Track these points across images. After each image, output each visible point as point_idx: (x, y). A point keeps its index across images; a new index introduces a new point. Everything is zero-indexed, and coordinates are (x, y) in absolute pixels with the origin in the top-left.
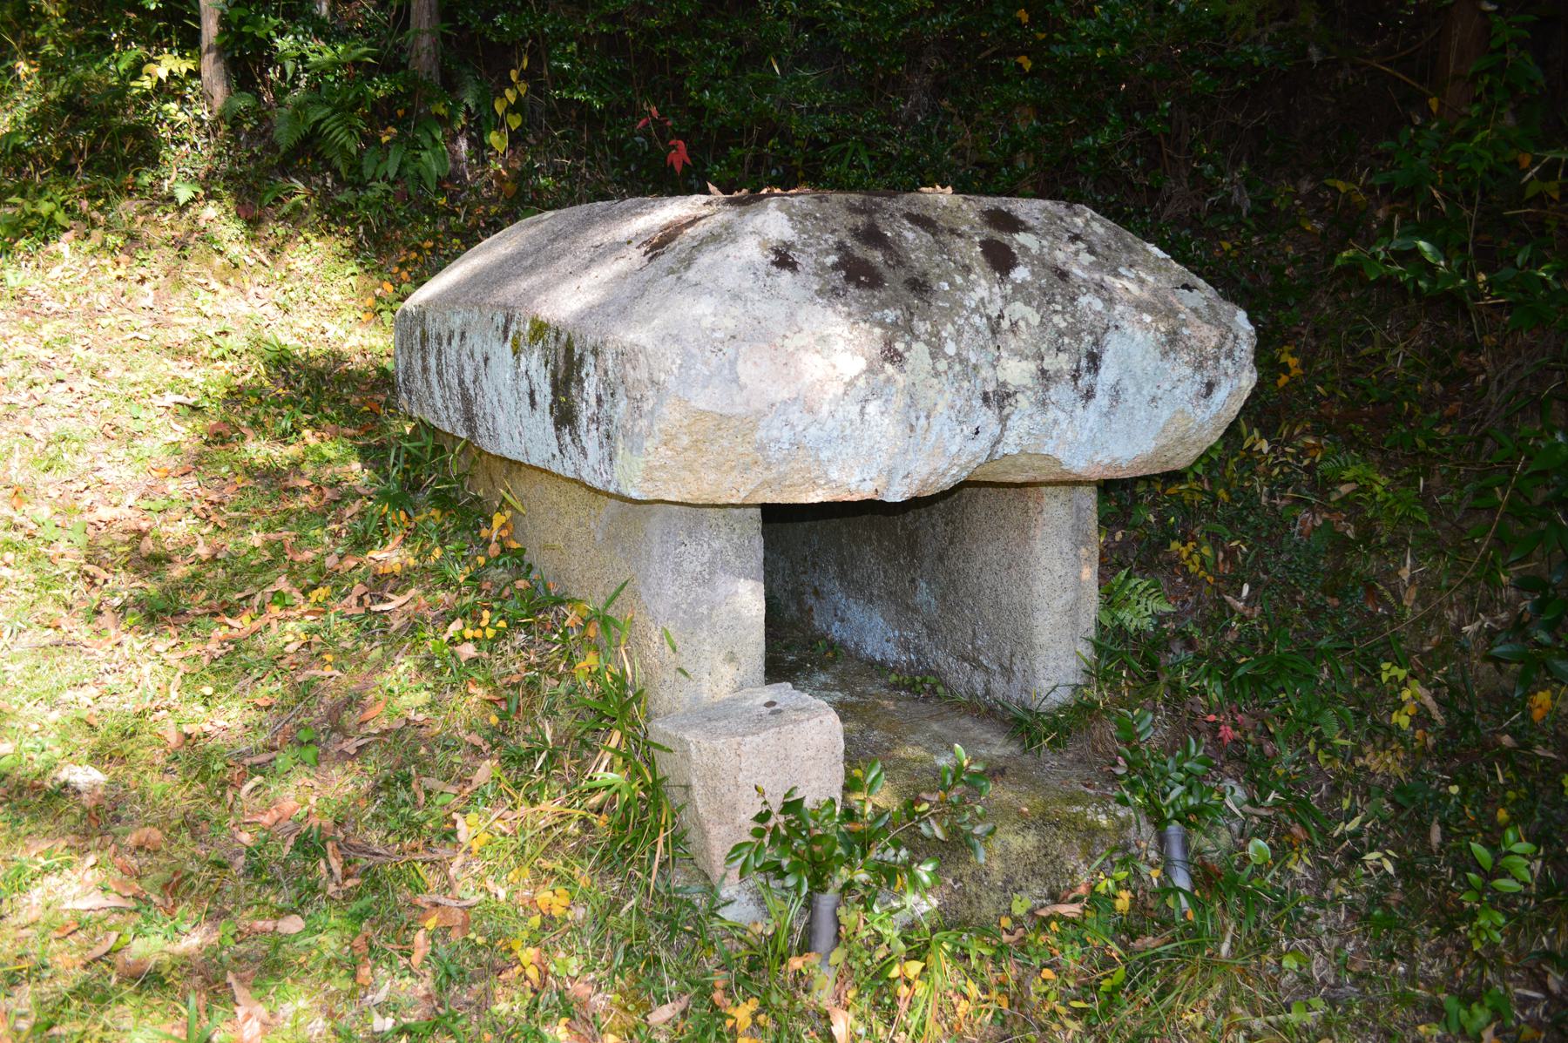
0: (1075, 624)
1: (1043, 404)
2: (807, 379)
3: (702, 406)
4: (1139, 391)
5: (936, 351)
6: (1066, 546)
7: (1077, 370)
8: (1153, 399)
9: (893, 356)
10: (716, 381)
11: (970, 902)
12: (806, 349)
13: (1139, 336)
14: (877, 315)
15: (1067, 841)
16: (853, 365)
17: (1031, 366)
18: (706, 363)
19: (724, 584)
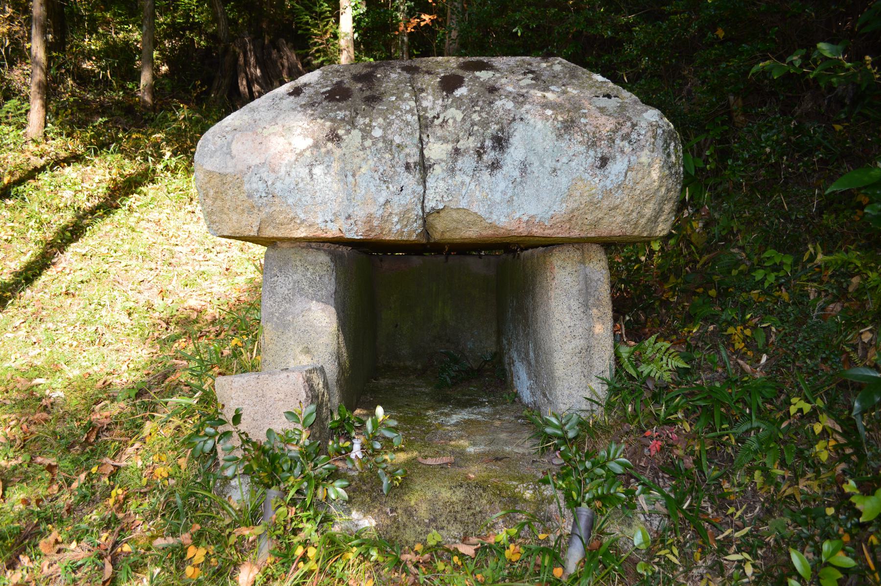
1: (452, 171)
2: (272, 151)
3: (209, 168)
4: (542, 164)
5: (366, 133)
6: (574, 304)
7: (482, 147)
8: (555, 170)
9: (334, 137)
10: (218, 153)
11: (398, 528)
12: (275, 134)
13: (540, 125)
14: (332, 115)
15: (491, 503)
16: (302, 143)
17: (449, 147)
18: (214, 144)
19: (300, 304)
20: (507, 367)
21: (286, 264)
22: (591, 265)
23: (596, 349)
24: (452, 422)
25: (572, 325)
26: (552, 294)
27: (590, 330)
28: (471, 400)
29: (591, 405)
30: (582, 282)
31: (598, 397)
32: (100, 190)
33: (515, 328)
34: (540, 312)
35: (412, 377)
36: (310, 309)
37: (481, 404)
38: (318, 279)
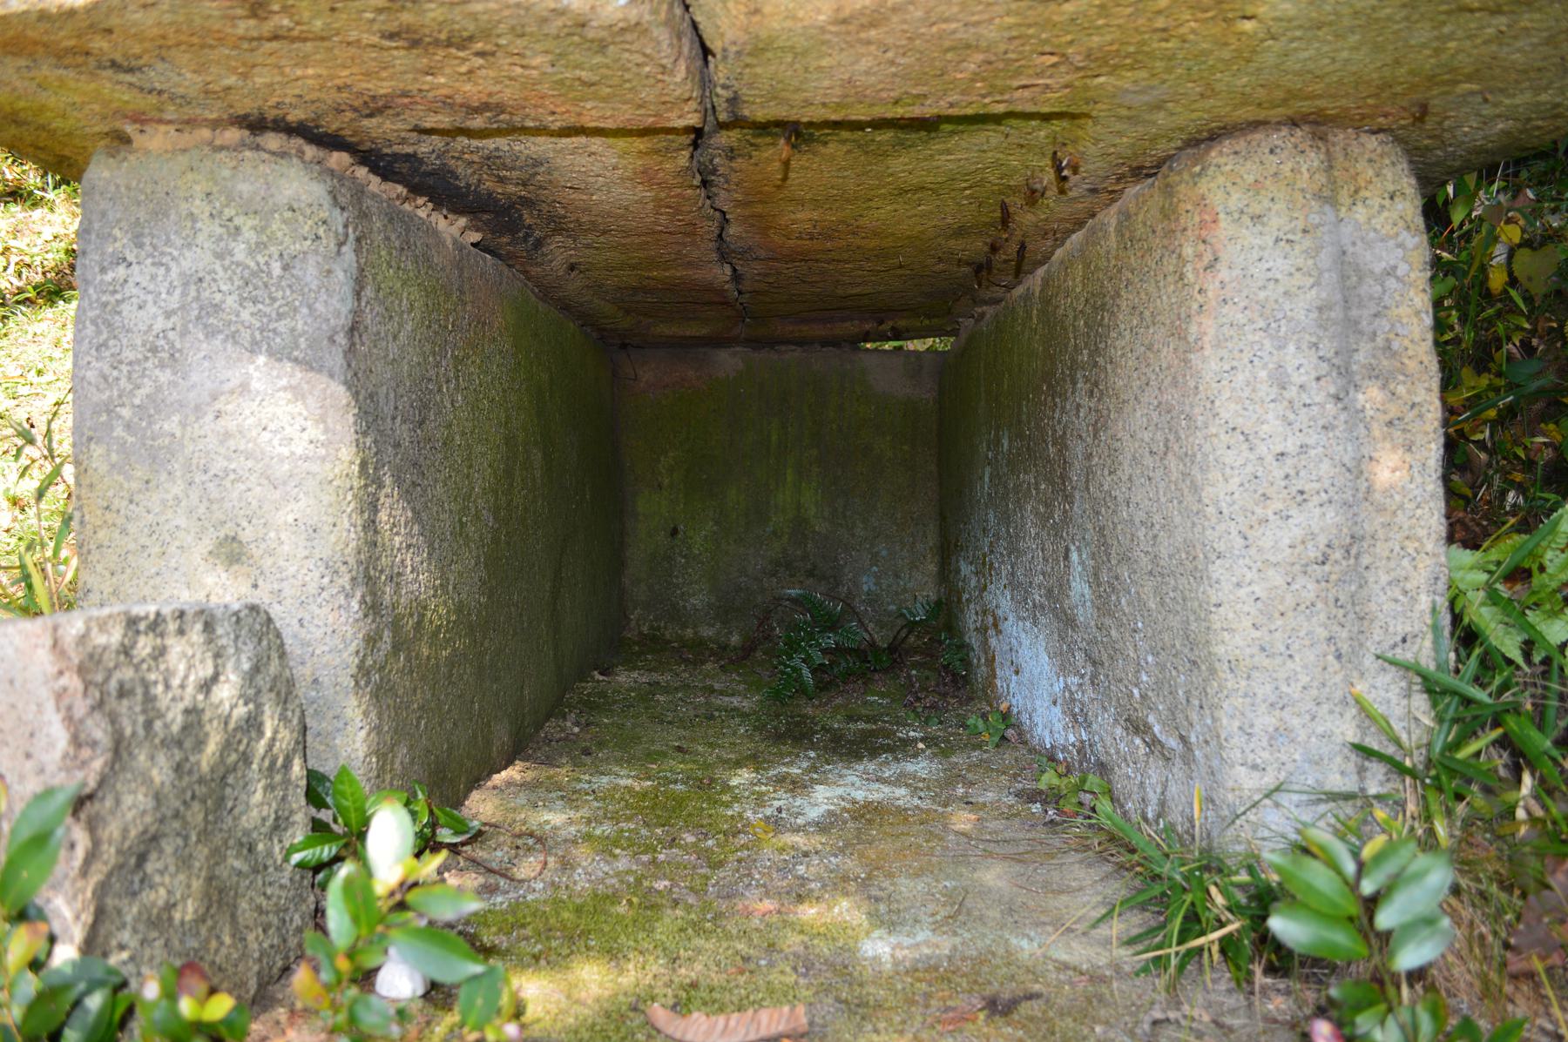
0: (1353, 610)
6: (1301, 364)
20: (973, 640)
21: (159, 213)
22: (1360, 213)
23: (1381, 549)
24: (814, 814)
25: (1291, 446)
26: (1206, 327)
27: (1357, 470)
28: (872, 733)
29: (1361, 771)
30: (1330, 278)
31: (1397, 742)
32: (49, 256)
33: (1006, 519)
34: (1135, 427)
35: (709, 666)
36: (244, 388)
37: (904, 748)
38: (276, 268)
